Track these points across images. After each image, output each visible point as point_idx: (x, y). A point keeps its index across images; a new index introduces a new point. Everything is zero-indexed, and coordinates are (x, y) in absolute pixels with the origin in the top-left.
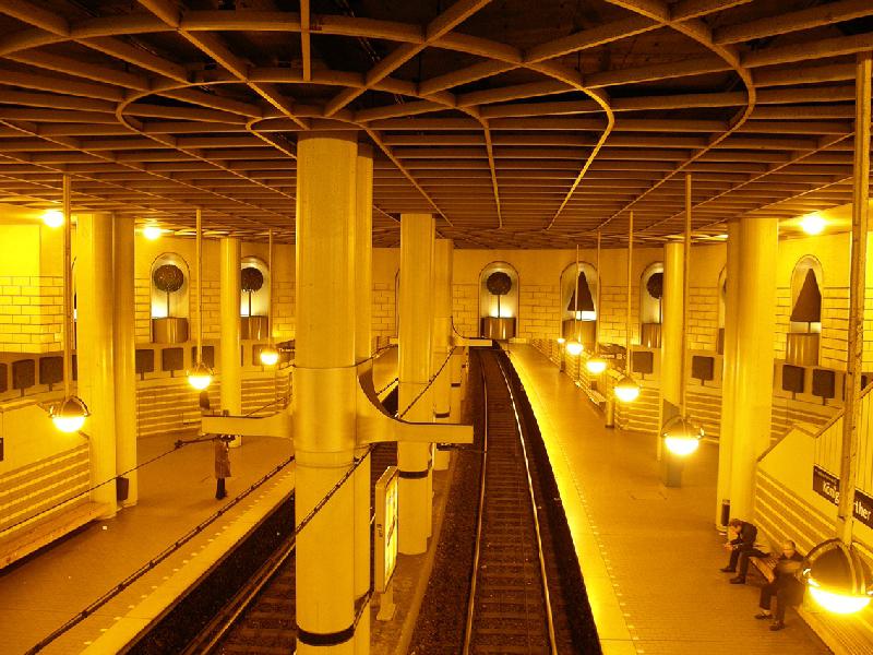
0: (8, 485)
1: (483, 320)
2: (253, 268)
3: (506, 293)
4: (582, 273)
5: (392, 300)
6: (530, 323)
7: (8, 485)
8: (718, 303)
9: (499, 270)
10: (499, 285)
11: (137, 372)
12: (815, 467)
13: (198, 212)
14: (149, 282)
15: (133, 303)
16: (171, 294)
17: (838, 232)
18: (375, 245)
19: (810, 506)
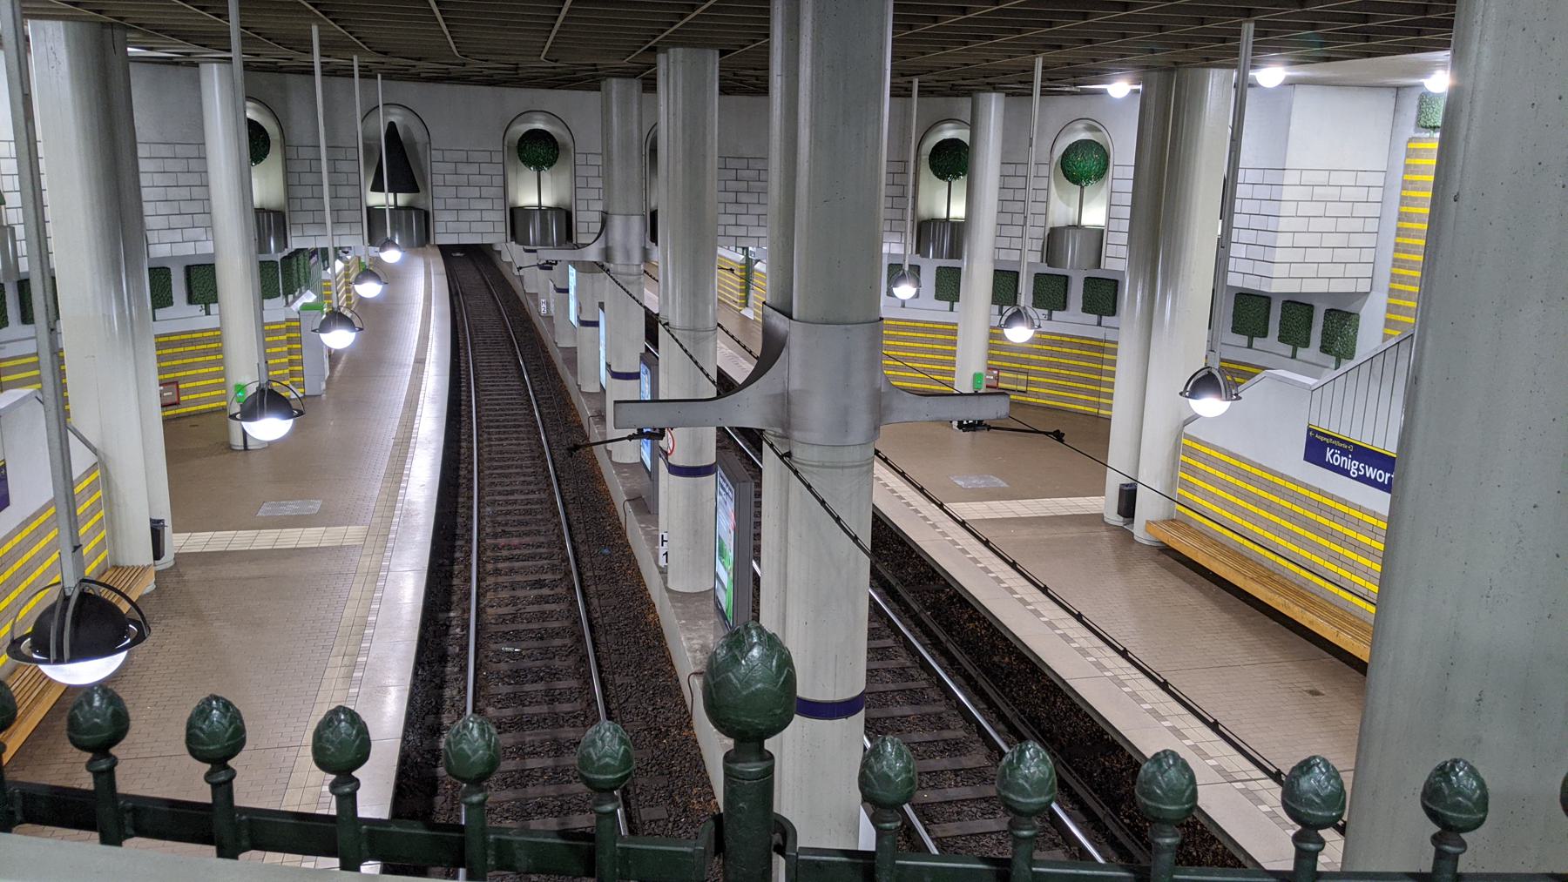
0: (13, 556)
1: (512, 210)
2: (1080, 141)
3: (550, 165)
4: (392, 126)
5: (498, 180)
6: (732, 220)
7: (13, 556)
8: (1048, 189)
9: (539, 126)
10: (539, 151)
11: (994, 302)
12: (1309, 430)
13: (315, 29)
14: (1114, 159)
15: (138, 188)
16: (545, 175)
17: (1137, 91)
18: (724, 91)
19: (1307, 486)
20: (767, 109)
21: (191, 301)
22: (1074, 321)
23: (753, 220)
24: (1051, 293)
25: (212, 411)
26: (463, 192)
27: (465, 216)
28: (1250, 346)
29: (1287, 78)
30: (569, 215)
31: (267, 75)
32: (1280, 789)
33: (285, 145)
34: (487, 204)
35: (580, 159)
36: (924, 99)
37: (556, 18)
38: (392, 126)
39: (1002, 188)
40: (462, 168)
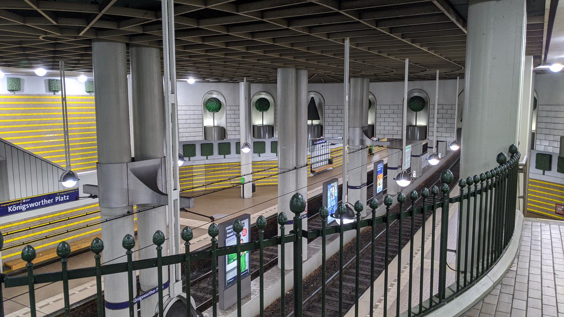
1: (253, 126)
2: (417, 97)
20: (343, 88)
21: (220, 154)
22: (216, 158)
23: (444, 130)
24: (207, 149)
25: (273, 185)
26: (335, 119)
27: (335, 128)
28: (544, 174)
29: (47, 72)
30: (322, 127)
31: (250, 82)
32: (264, 274)
33: (275, 106)
34: (395, 124)
35: (378, 107)
36: (442, 81)
37: (542, 50)
38: (312, 98)
39: (239, 114)
40: (335, 111)
